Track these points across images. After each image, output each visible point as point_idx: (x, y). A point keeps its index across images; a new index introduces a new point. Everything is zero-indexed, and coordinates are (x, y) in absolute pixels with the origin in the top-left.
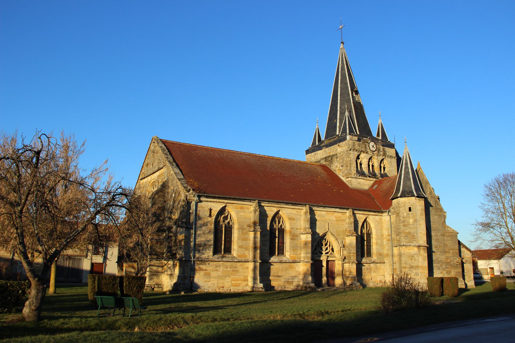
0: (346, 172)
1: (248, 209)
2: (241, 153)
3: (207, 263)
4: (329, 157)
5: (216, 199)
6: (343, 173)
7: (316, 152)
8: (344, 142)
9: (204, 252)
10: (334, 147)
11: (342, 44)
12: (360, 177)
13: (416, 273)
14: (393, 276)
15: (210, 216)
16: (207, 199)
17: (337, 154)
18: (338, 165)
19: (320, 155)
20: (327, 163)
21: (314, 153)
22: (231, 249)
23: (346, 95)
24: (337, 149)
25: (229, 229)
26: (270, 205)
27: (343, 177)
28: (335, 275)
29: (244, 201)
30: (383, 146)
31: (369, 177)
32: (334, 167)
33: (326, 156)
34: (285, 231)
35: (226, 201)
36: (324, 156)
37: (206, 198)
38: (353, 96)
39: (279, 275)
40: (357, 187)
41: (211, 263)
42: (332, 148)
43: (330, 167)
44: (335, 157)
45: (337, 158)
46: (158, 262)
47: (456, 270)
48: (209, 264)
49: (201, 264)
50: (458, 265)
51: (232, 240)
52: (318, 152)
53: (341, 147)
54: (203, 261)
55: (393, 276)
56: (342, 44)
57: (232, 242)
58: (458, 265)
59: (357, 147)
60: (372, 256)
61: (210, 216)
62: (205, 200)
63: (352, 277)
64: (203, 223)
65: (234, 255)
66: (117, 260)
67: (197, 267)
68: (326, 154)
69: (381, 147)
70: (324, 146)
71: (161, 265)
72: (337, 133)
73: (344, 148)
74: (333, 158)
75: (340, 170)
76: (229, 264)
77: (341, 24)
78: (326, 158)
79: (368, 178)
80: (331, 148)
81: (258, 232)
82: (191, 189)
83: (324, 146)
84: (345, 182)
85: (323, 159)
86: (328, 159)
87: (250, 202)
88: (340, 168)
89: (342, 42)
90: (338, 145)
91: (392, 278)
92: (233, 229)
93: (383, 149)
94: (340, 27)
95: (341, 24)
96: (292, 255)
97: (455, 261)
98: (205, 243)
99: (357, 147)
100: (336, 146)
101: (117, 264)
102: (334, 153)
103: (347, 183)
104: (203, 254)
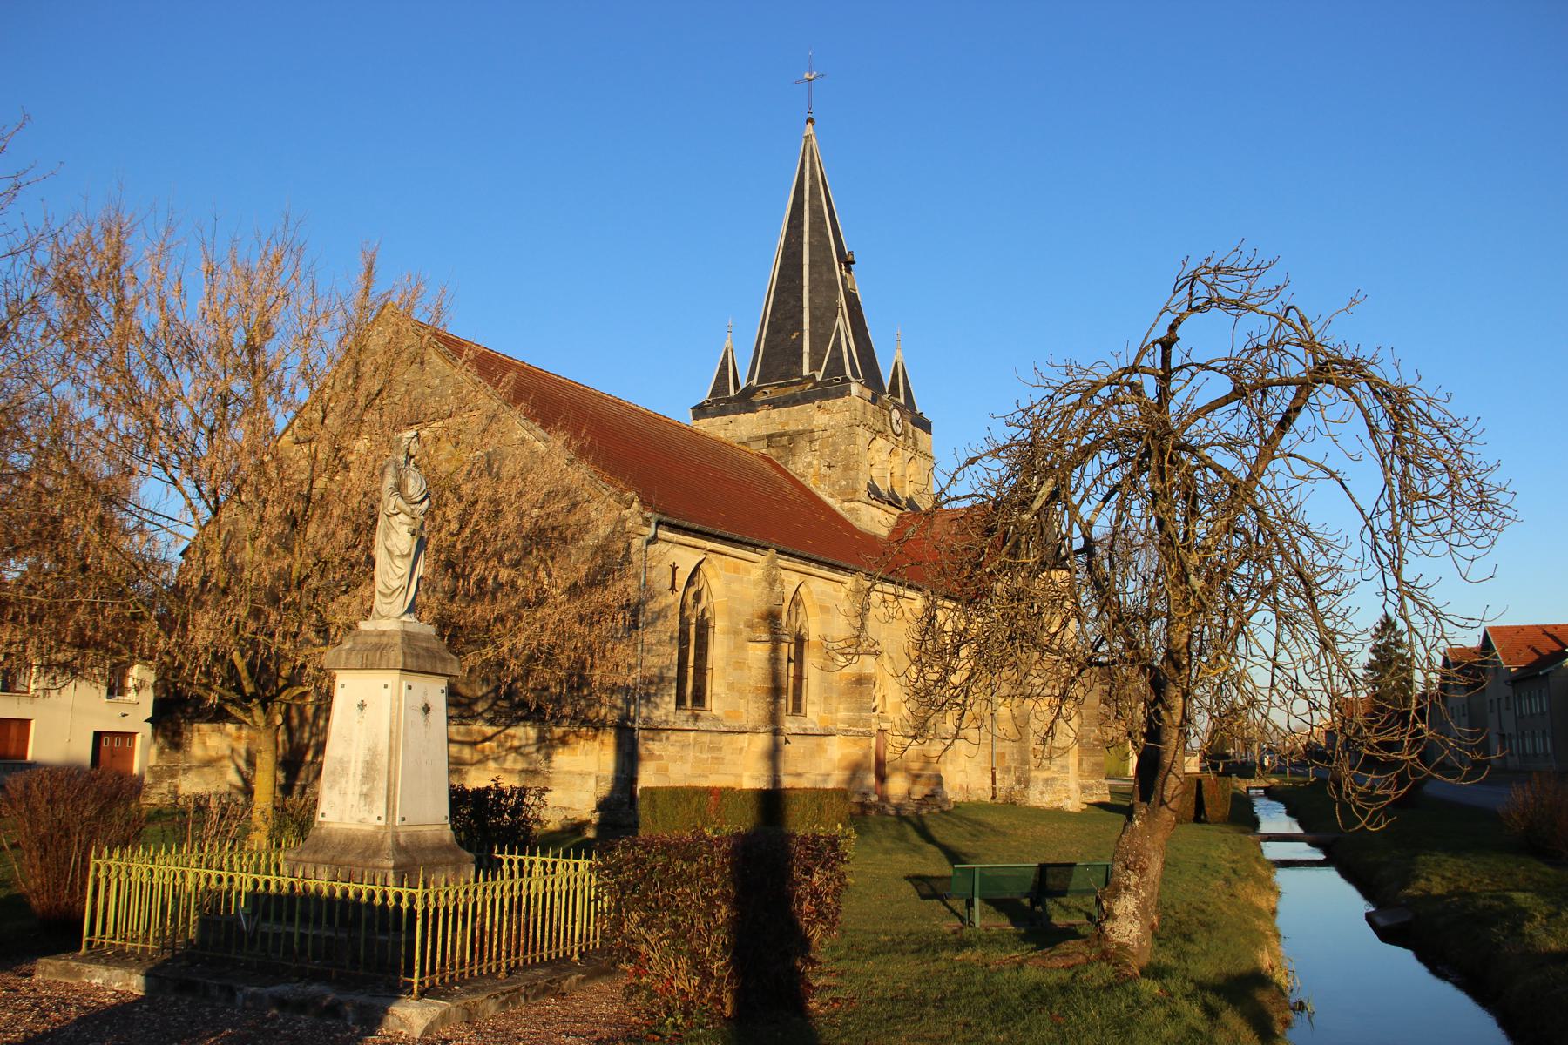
0: (844, 483)
1: (748, 572)
2: (601, 397)
3: (664, 735)
4: (781, 435)
5: (689, 535)
6: (833, 485)
7: (731, 417)
8: (840, 401)
9: (658, 700)
10: (803, 411)
11: (810, 124)
12: (874, 502)
13: (1062, 767)
14: (994, 774)
15: (673, 588)
16: (670, 534)
17: (812, 431)
18: (815, 462)
19: (742, 428)
20: (773, 451)
21: (725, 419)
22: (704, 694)
23: (825, 268)
24: (812, 416)
25: (703, 628)
26: (791, 567)
27: (832, 496)
28: (887, 769)
29: (744, 547)
30: (913, 424)
31: (890, 503)
32: (800, 465)
33: (769, 432)
34: (806, 644)
35: (710, 545)
36: (763, 431)
37: (670, 531)
38: (841, 273)
39: (800, 771)
40: (869, 528)
41: (674, 737)
42: (794, 412)
43: (786, 463)
44: (808, 439)
45: (811, 442)
46: (462, 728)
47: (1093, 760)
48: (667, 738)
49: (653, 740)
50: (1098, 745)
51: (709, 666)
52: (742, 417)
53: (828, 412)
54: (656, 730)
55: (994, 774)
56: (810, 124)
57: (709, 672)
58: (1098, 745)
59: (870, 420)
60: (803, 712)
61: (673, 588)
62: (667, 538)
63: (930, 777)
64: (657, 610)
65: (715, 712)
66: (150, 715)
67: (642, 751)
68: (770, 427)
69: (910, 426)
70: (763, 403)
71: (468, 739)
72: (806, 372)
73: (840, 417)
74: (797, 439)
75: (821, 477)
76: (707, 737)
77: (810, 67)
78: (770, 437)
79: (886, 507)
80: (789, 412)
81: (782, 644)
82: (637, 499)
83: (763, 403)
84: (840, 511)
85: (759, 439)
86: (779, 442)
87: (755, 552)
88: (822, 471)
89: (810, 120)
90: (819, 407)
91: (989, 782)
92: (711, 631)
93: (914, 432)
94: (807, 75)
95: (810, 67)
96: (822, 714)
97: (1092, 735)
98: (661, 673)
99: (870, 420)
100: (810, 408)
101: (149, 725)
102: (800, 427)
103: (847, 516)
104: (657, 707)
